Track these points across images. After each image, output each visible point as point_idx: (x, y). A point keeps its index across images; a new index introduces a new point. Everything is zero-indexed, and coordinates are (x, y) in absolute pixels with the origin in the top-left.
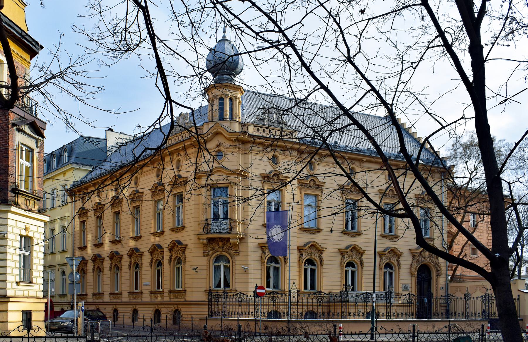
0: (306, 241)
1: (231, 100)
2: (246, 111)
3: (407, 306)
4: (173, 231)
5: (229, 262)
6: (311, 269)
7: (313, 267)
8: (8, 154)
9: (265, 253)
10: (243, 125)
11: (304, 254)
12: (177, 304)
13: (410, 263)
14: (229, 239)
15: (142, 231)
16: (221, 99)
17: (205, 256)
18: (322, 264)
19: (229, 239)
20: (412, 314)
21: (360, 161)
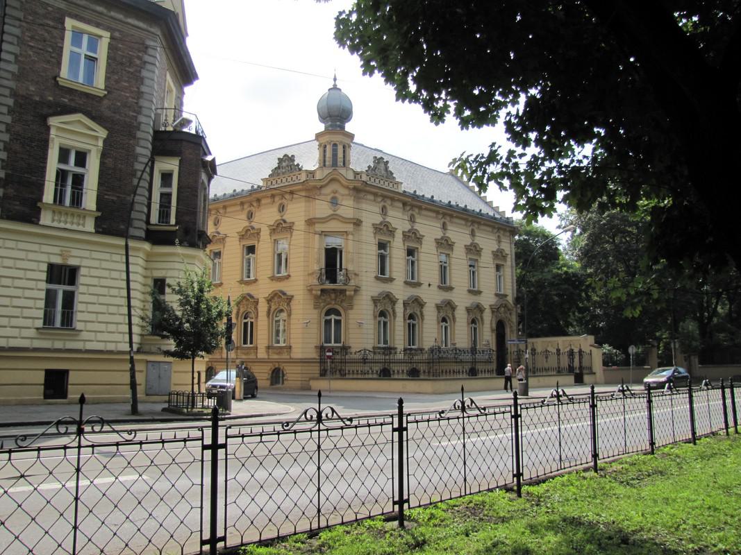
0: (380, 290)
1: (344, 147)
2: (359, 163)
3: (409, 362)
4: (272, 280)
5: (341, 315)
6: (335, 320)
7: (337, 318)
8: (197, 192)
9: (376, 306)
10: (356, 174)
11: (408, 308)
12: (278, 362)
13: (490, 318)
14: (345, 290)
15: (224, 278)
16: (335, 145)
17: (315, 308)
18: (423, 319)
19: (345, 290)
20: (493, 371)
21: (451, 216)
